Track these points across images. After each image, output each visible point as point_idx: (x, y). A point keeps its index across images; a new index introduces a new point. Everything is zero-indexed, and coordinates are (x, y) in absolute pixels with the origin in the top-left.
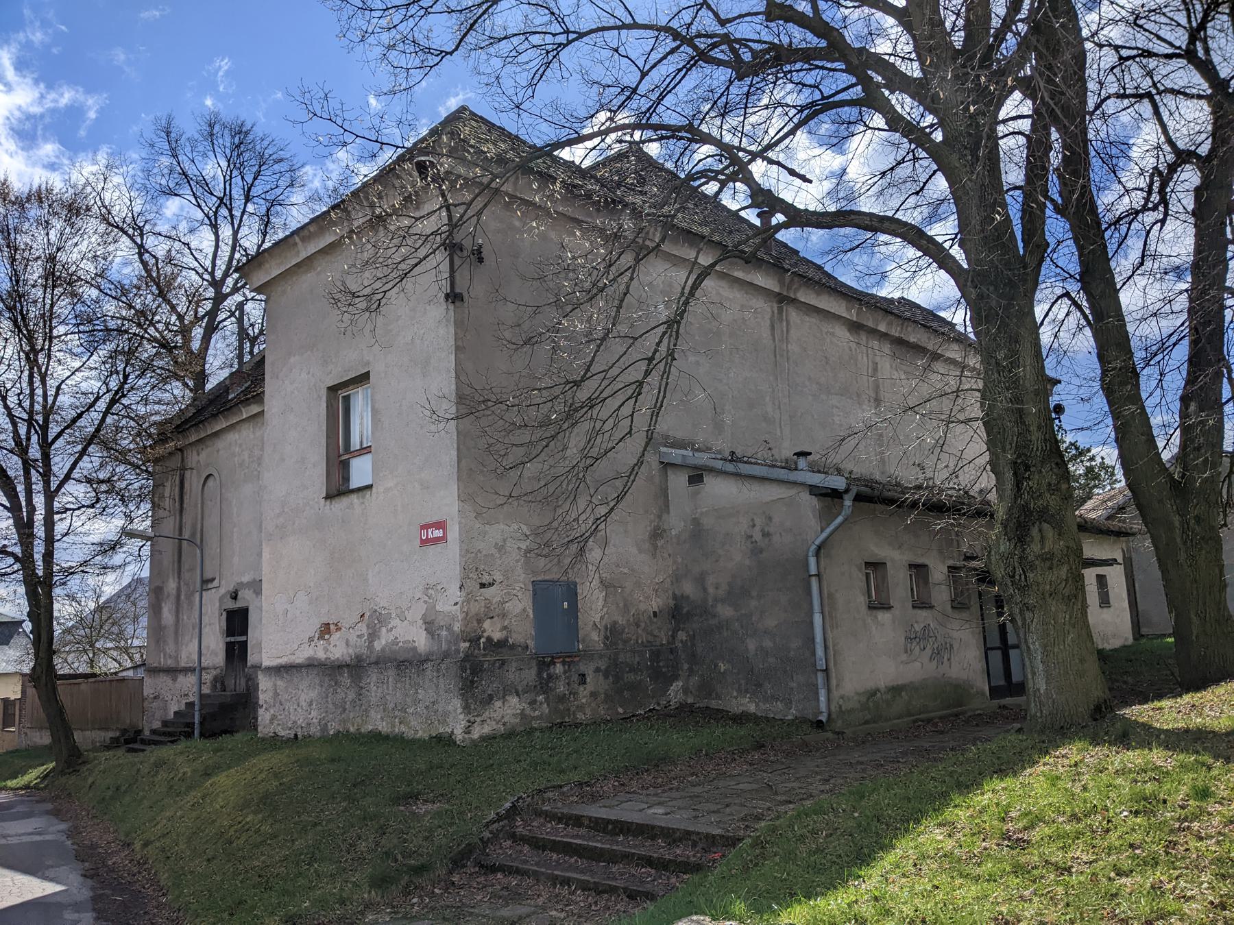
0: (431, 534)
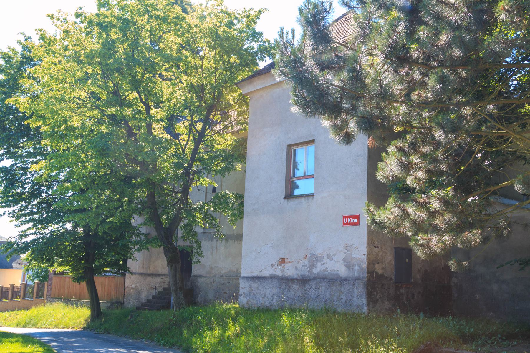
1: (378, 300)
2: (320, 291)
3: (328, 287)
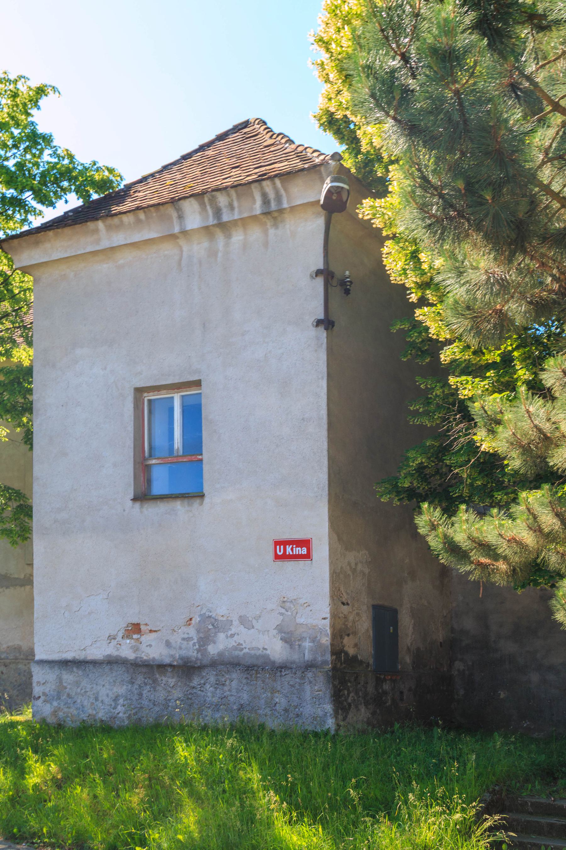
0: (292, 550)
1: (350, 705)
2: (226, 688)
3: (244, 681)
